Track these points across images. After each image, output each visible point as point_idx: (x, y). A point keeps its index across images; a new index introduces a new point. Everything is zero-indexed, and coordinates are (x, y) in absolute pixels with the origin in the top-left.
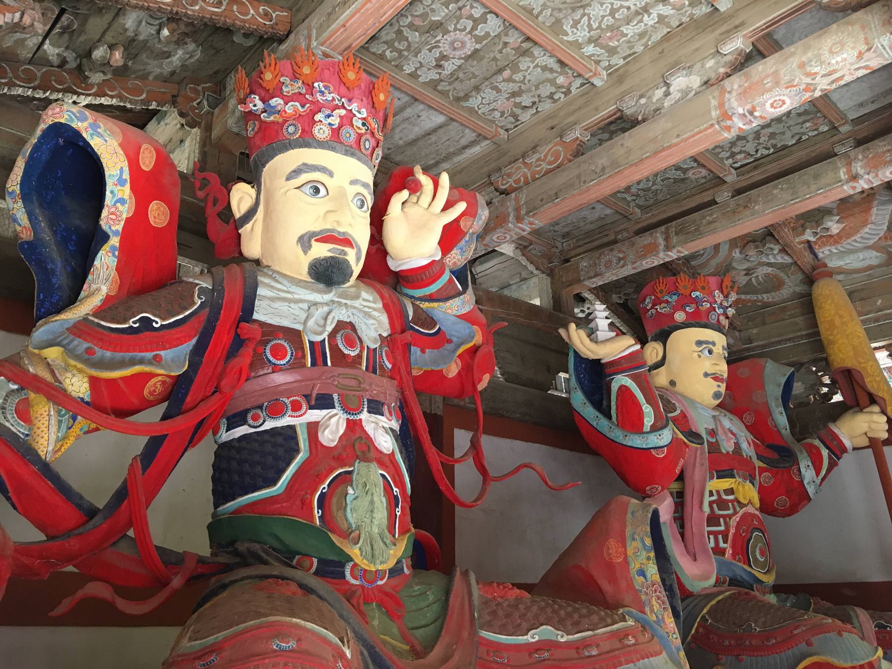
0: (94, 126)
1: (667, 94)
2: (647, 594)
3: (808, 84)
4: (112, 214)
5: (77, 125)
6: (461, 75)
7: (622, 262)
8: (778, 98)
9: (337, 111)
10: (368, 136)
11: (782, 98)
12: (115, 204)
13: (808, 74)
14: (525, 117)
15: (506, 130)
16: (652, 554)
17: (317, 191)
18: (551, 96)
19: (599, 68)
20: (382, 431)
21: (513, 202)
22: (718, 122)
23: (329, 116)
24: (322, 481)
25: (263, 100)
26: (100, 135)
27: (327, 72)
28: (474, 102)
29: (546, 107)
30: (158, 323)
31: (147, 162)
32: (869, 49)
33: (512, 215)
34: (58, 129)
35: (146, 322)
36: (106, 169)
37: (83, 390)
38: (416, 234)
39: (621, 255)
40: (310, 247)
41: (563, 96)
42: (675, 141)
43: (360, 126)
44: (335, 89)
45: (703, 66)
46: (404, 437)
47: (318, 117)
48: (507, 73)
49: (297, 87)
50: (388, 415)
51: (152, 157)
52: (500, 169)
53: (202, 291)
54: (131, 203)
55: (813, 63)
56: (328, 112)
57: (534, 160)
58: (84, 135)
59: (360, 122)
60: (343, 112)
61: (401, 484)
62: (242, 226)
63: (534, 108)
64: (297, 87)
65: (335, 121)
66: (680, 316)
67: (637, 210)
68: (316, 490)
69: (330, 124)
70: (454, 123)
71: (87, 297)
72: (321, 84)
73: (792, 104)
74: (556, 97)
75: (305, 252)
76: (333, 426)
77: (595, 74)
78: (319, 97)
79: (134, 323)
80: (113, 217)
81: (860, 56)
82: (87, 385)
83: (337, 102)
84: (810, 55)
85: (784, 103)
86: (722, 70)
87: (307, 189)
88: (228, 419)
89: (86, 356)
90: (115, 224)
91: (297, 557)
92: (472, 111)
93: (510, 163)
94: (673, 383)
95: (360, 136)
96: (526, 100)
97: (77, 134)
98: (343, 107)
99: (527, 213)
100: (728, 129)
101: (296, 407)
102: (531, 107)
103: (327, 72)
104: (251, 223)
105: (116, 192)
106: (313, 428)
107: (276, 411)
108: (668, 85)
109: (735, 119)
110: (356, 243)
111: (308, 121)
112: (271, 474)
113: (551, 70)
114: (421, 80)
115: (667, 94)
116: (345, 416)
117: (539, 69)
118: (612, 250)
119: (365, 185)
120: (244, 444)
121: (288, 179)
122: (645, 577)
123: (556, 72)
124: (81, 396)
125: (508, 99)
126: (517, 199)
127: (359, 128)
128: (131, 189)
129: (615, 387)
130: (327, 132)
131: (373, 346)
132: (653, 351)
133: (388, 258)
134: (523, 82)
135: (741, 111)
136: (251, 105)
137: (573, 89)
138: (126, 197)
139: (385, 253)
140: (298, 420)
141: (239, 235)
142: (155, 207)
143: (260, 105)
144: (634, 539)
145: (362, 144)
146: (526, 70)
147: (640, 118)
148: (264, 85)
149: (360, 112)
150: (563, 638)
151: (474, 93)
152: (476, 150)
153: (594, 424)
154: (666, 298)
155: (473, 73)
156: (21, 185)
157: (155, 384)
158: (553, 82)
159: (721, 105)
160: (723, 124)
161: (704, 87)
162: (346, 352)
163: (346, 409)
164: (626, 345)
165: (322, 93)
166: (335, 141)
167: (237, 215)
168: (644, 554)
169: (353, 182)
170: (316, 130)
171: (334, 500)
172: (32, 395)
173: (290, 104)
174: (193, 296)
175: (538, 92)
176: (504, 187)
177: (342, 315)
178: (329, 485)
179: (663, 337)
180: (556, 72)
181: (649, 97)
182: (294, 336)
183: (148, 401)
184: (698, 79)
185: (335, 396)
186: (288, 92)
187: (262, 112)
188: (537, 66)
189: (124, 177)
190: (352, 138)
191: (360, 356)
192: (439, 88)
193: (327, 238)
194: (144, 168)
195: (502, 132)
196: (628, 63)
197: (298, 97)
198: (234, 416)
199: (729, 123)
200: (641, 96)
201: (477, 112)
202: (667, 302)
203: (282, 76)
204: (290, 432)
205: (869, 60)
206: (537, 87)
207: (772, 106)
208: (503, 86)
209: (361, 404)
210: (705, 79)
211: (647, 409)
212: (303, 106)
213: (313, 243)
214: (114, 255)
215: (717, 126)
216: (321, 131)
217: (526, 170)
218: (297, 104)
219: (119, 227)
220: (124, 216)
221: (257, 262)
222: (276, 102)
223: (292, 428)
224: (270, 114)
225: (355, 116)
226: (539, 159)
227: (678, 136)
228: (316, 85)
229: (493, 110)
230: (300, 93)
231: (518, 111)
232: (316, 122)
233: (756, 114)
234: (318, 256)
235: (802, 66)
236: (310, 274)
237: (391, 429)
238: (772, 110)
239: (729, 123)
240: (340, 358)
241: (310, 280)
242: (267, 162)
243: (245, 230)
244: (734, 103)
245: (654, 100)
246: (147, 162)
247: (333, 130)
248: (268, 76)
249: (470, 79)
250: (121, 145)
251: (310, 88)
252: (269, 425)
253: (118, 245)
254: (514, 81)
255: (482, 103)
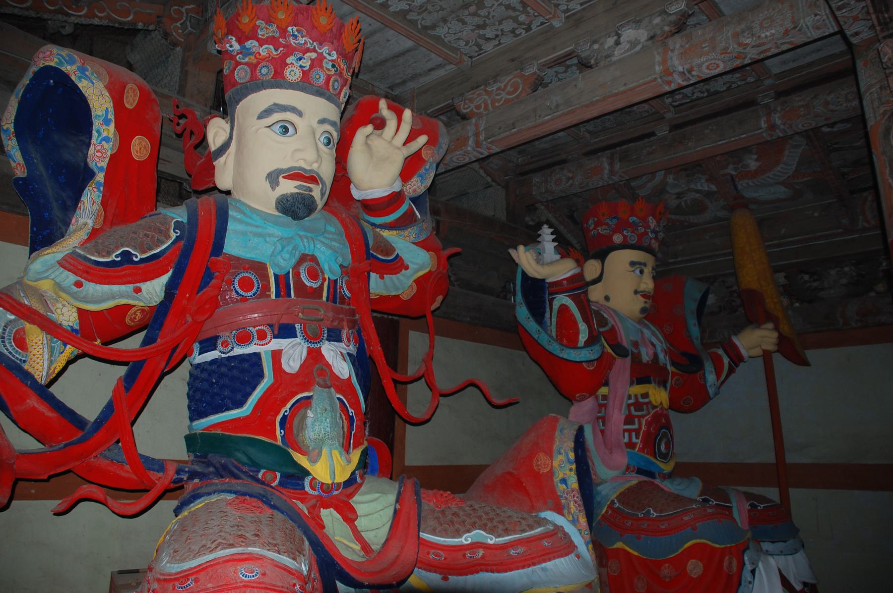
0: (82, 70)
1: (617, 43)
2: (566, 498)
3: (740, 53)
4: (98, 151)
5: (67, 69)
6: (429, 7)
7: (571, 181)
8: (713, 61)
9: (308, 54)
10: (338, 78)
11: (717, 62)
12: (101, 142)
13: (740, 44)
14: (489, 47)
15: (471, 57)
16: (574, 467)
17: (286, 130)
18: (513, 31)
19: (558, 12)
20: (337, 358)
21: (473, 128)
22: (661, 77)
23: (300, 59)
24: (284, 403)
25: (240, 41)
26: (87, 78)
27: (300, 17)
28: (441, 31)
29: (508, 40)
30: (139, 256)
31: (131, 101)
32: (795, 28)
33: (471, 139)
34: (48, 72)
35: (126, 255)
36: (93, 110)
37: (72, 319)
38: (379, 164)
39: (570, 175)
40: (278, 184)
41: (524, 32)
42: (622, 89)
43: (330, 67)
44: (307, 32)
45: (650, 22)
46: (360, 361)
47: (289, 60)
48: (473, 9)
49: (272, 30)
50: (346, 341)
51: (135, 96)
52: (463, 94)
53: (178, 225)
54: (115, 140)
55: (745, 34)
56: (300, 55)
57: (495, 88)
58: (73, 78)
59: (331, 63)
60: (314, 55)
61: (356, 404)
62: (216, 159)
63: (497, 39)
64: (272, 30)
65: (306, 64)
66: (617, 239)
67: (587, 135)
68: (278, 413)
69: (301, 66)
70: (421, 48)
71: (75, 231)
72: (295, 29)
73: (725, 67)
74: (517, 32)
75: (273, 189)
76: (293, 353)
77: (554, 17)
78: (292, 41)
79: (117, 256)
80: (99, 154)
81: (786, 32)
82: (76, 314)
83: (309, 45)
84: (743, 26)
85: (718, 66)
86: (667, 28)
87: (277, 128)
88: (200, 343)
89: (75, 289)
90: (101, 161)
91: (263, 471)
92: (438, 39)
93: (472, 89)
94: (607, 298)
95: (328, 78)
96: (489, 33)
97: (66, 77)
98: (314, 50)
99: (486, 139)
100: (669, 83)
101: (262, 336)
102: (494, 39)
103: (300, 17)
104: (224, 157)
105: (102, 131)
106: (276, 355)
107: (244, 339)
108: (619, 36)
109: (675, 75)
110: (321, 179)
111: (280, 65)
112: (239, 396)
113: (514, 9)
114: (392, 9)
115: (617, 43)
116: (306, 345)
117: (503, 8)
118: (562, 169)
119: (333, 124)
120: (214, 367)
121: (260, 117)
122: (566, 485)
123: (519, 11)
124: (71, 324)
125: (473, 31)
126: (477, 125)
127: (329, 70)
128: (116, 127)
129: (556, 305)
130: (298, 74)
131: (333, 278)
132: (592, 269)
133: (352, 186)
134: (487, 17)
135: (680, 69)
136: (228, 45)
137: (533, 27)
138: (111, 136)
139: (348, 182)
140: (264, 349)
141: (214, 167)
142: (138, 142)
143: (236, 46)
144: (560, 454)
145: (331, 84)
146: (491, 7)
147: (592, 62)
148: (241, 27)
149: (330, 55)
150: (492, 540)
151: (441, 24)
152: (442, 72)
153: (536, 337)
154: (607, 221)
155: (441, 6)
156: (15, 123)
157: (135, 313)
158: (515, 19)
159: (664, 62)
160: (665, 78)
161: (650, 42)
162: (308, 284)
163: (308, 338)
164: (564, 270)
165: (295, 37)
166: (305, 84)
167: (213, 148)
168: (568, 466)
169: (322, 121)
170: (287, 72)
171: (296, 421)
172: (28, 326)
173: (264, 47)
174: (168, 230)
175: (501, 27)
176: (465, 111)
177: (307, 248)
178: (290, 409)
179: (602, 256)
180: (519, 11)
181: (602, 44)
182: (260, 268)
183: (130, 327)
184: (646, 34)
185: (298, 326)
186: (263, 35)
187: (238, 54)
188: (501, 4)
189: (109, 117)
190: (321, 80)
191: (321, 287)
192: (408, 17)
193: (295, 175)
194: (128, 106)
195: (466, 58)
196: (584, 9)
197: (272, 40)
198: (207, 340)
199: (670, 78)
200: (595, 42)
201: (443, 40)
202: (607, 224)
203: (259, 19)
204: (254, 359)
205: (793, 37)
206: (500, 23)
207: (708, 68)
208: (469, 20)
209: (321, 333)
210: (652, 34)
211: (583, 327)
212: (276, 50)
213: (281, 179)
214: (99, 190)
215: (659, 80)
216: (293, 73)
217: (487, 97)
218: (271, 47)
219: (104, 164)
220: (109, 153)
221: (228, 193)
222: (251, 44)
223: (257, 355)
224: (245, 56)
225: (325, 58)
226: (499, 89)
227: (625, 85)
228: (290, 29)
229: (459, 39)
230: (274, 37)
231: (481, 41)
232: (287, 65)
233: (694, 73)
234: (284, 192)
235: (736, 35)
236: (277, 208)
237: (349, 354)
238: (707, 71)
239: (670, 78)
240: (301, 289)
241: (277, 213)
242: (241, 100)
243: (219, 163)
244: (676, 62)
245: (606, 47)
246: (131, 100)
247: (304, 72)
248: (246, 20)
249: (437, 12)
250: (106, 87)
251: (284, 32)
252: (238, 351)
253: (102, 180)
254: (479, 16)
255: (448, 33)
